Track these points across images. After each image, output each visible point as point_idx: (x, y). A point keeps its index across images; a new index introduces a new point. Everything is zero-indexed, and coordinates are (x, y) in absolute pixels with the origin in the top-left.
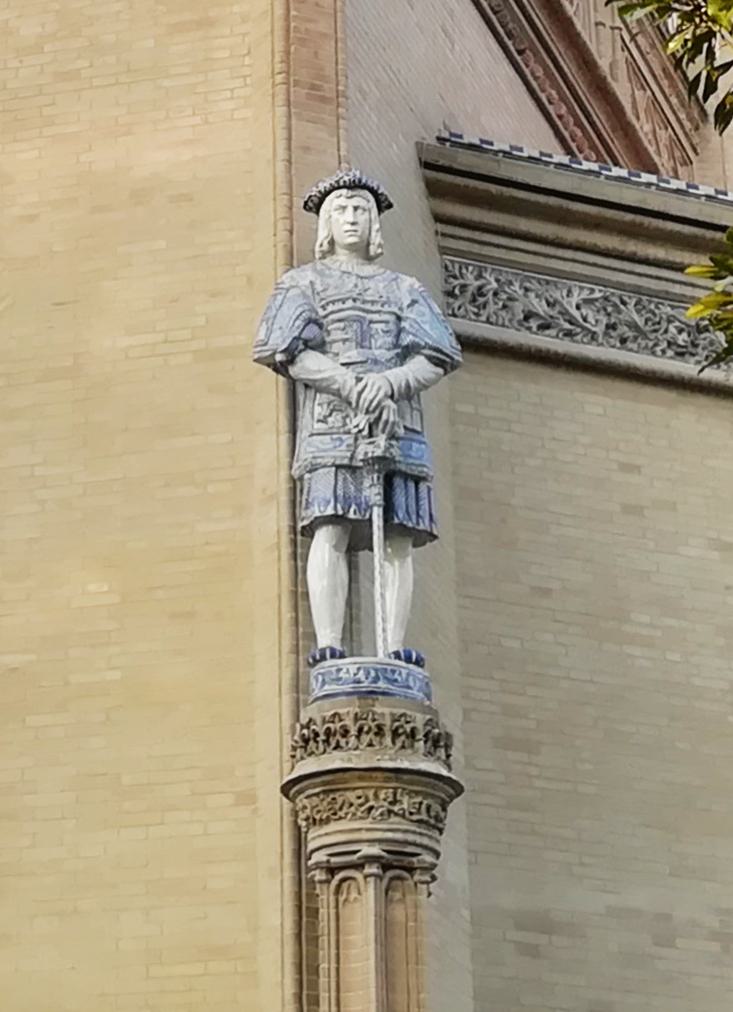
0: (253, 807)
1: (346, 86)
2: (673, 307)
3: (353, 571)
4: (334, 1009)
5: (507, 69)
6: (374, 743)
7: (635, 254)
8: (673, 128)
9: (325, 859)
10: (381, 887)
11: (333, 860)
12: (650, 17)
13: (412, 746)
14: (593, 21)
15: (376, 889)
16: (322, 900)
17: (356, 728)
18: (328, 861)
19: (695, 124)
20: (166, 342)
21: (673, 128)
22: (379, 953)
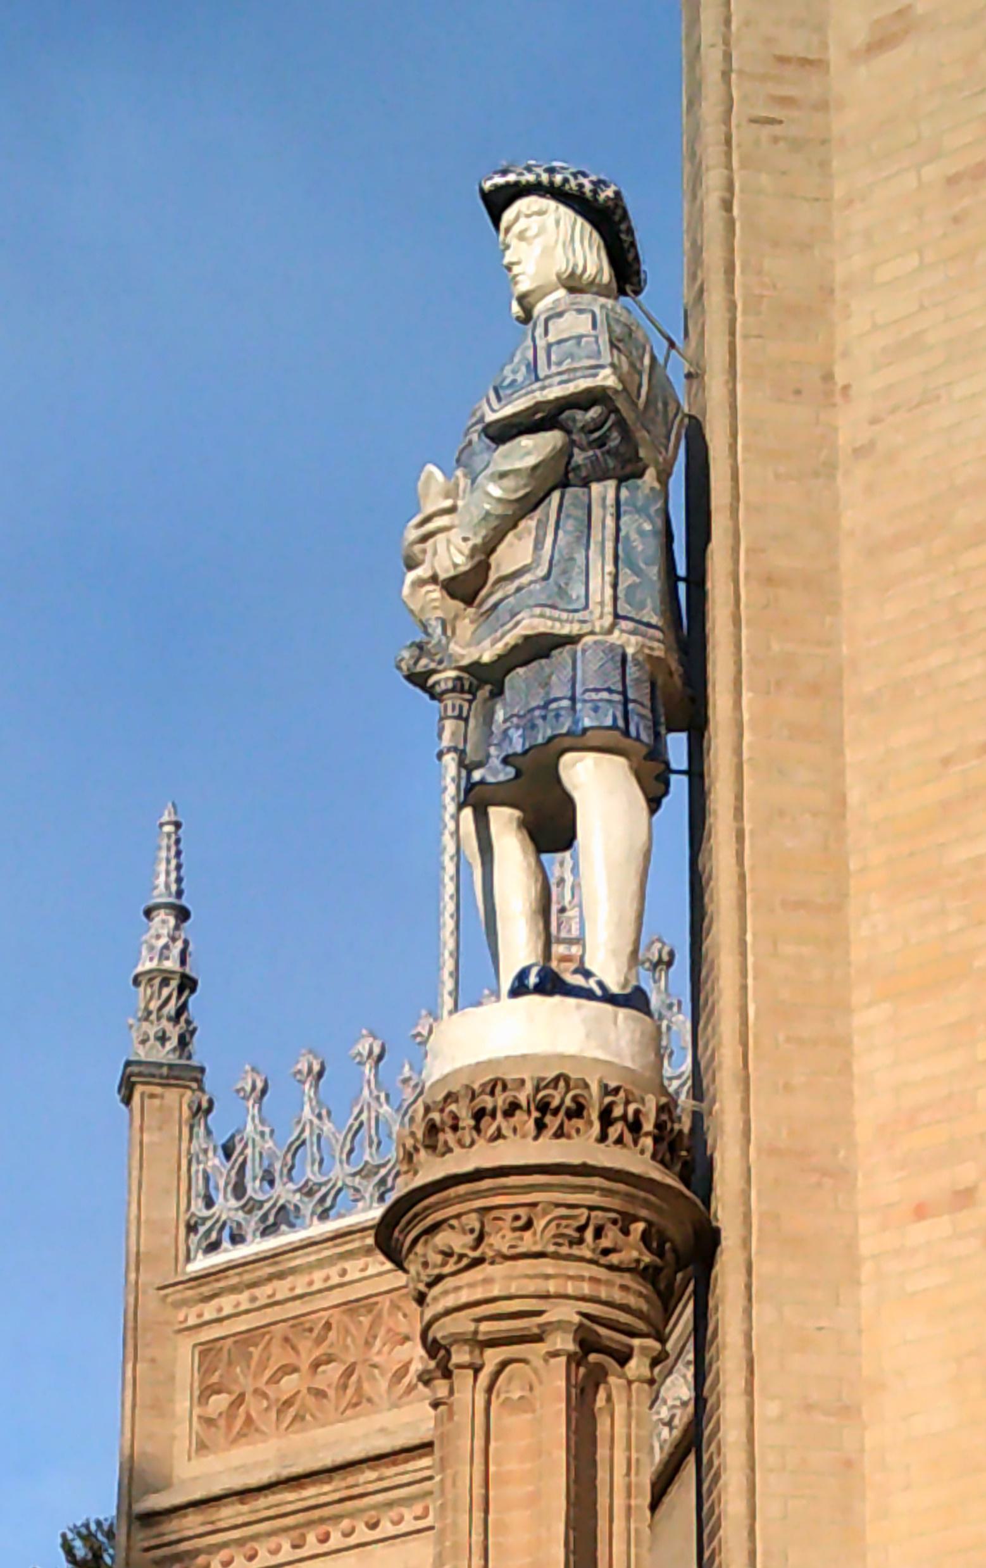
0: (648, 1126)
1: (669, 1040)
2: (239, 1274)
3: (492, 545)
4: (477, 1561)
5: (673, 1493)
6: (504, 1132)
7: (242, 1503)
8: (189, 1170)
9: (472, 1327)
10: (659, 988)
11: (484, 1327)
12: (560, 1240)
13: (636, 1143)
14: (183, 1217)
15: (596, 1060)
16: (570, 918)
17: (322, 1387)
18: (476, 1332)
19: (489, 703)
20: (875, 327)
21: (189, 1170)
22: (572, 1444)
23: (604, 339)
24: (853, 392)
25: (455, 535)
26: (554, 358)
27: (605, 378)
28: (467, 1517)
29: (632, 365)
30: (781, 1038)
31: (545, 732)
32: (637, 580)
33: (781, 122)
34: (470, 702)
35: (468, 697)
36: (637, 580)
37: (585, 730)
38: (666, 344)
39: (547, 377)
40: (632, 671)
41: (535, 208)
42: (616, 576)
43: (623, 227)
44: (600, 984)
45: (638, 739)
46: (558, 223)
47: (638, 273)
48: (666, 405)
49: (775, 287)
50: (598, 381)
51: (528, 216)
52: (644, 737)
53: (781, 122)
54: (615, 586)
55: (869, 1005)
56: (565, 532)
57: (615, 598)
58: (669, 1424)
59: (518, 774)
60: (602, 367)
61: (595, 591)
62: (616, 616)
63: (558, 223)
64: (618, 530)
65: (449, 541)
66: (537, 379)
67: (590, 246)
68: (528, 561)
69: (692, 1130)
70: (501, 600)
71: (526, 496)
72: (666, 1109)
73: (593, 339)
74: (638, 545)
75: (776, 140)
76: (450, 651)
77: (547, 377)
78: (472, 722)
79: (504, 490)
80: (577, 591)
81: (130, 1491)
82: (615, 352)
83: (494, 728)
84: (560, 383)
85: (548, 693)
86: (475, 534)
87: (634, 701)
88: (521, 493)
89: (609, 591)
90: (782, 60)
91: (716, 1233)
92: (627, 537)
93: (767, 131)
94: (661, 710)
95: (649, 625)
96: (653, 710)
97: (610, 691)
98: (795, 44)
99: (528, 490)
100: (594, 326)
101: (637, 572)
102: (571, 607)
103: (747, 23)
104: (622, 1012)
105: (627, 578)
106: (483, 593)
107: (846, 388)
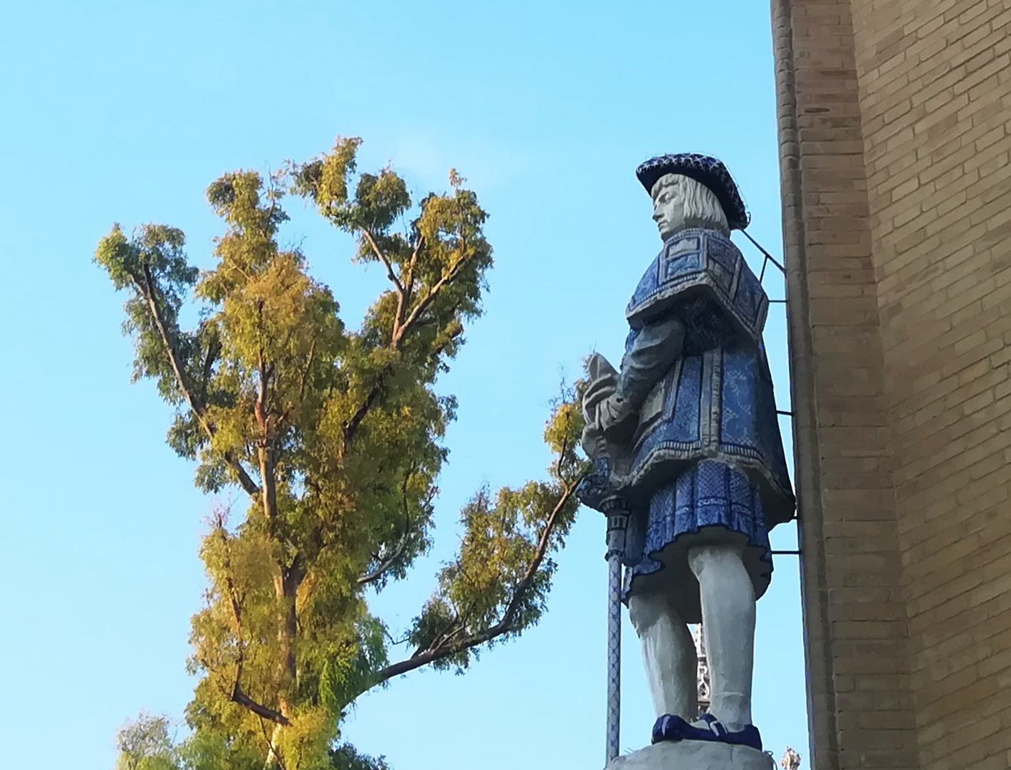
23: (703, 256)
24: (404, 679)
25: (612, 399)
26: (670, 271)
27: (702, 279)
28: (977, 59)
29: (725, 270)
30: (863, 759)
31: (324, 469)
32: (649, 549)
33: (828, 110)
34: (628, 516)
35: (627, 512)
36: (649, 549)
37: (700, 528)
38: (764, 256)
39: (664, 284)
40: (734, 481)
41: (670, 181)
42: (720, 414)
43: (728, 185)
44: (718, 726)
45: (739, 531)
46: (685, 189)
47: (744, 213)
48: (753, 294)
49: (828, 211)
50: (697, 282)
51: (667, 186)
52: (744, 529)
53: (828, 110)
54: (719, 422)
55: (931, 723)
56: (684, 388)
57: (720, 430)
58: (243, 686)
59: (663, 566)
60: (699, 272)
61: (604, 410)
62: (720, 442)
63: (685, 189)
64: (722, 382)
65: (608, 403)
66: (658, 286)
67: (708, 202)
68: (660, 410)
69: (646, 422)
70: (644, 440)
71: (658, 365)
72: (272, 536)
73: (696, 256)
74: (736, 391)
75: (824, 121)
76: (611, 480)
77: (664, 284)
78: (629, 532)
79: (642, 363)
80: (693, 427)
81: (805, 319)
82: (711, 262)
83: (131, 276)
84: (671, 287)
85: (959, 21)
86: (626, 397)
87: (736, 503)
88: (653, 364)
89: (714, 424)
90: (826, 73)
91: (756, 729)
92: (728, 387)
93: (817, 117)
94: (758, 505)
95: (745, 447)
96: (752, 508)
97: (716, 498)
98: (834, 63)
99: (658, 361)
100: (698, 248)
101: (735, 408)
102: (688, 440)
103: (802, 54)
104: (737, 748)
105: (729, 415)
106: (635, 436)
107: (405, 676)
